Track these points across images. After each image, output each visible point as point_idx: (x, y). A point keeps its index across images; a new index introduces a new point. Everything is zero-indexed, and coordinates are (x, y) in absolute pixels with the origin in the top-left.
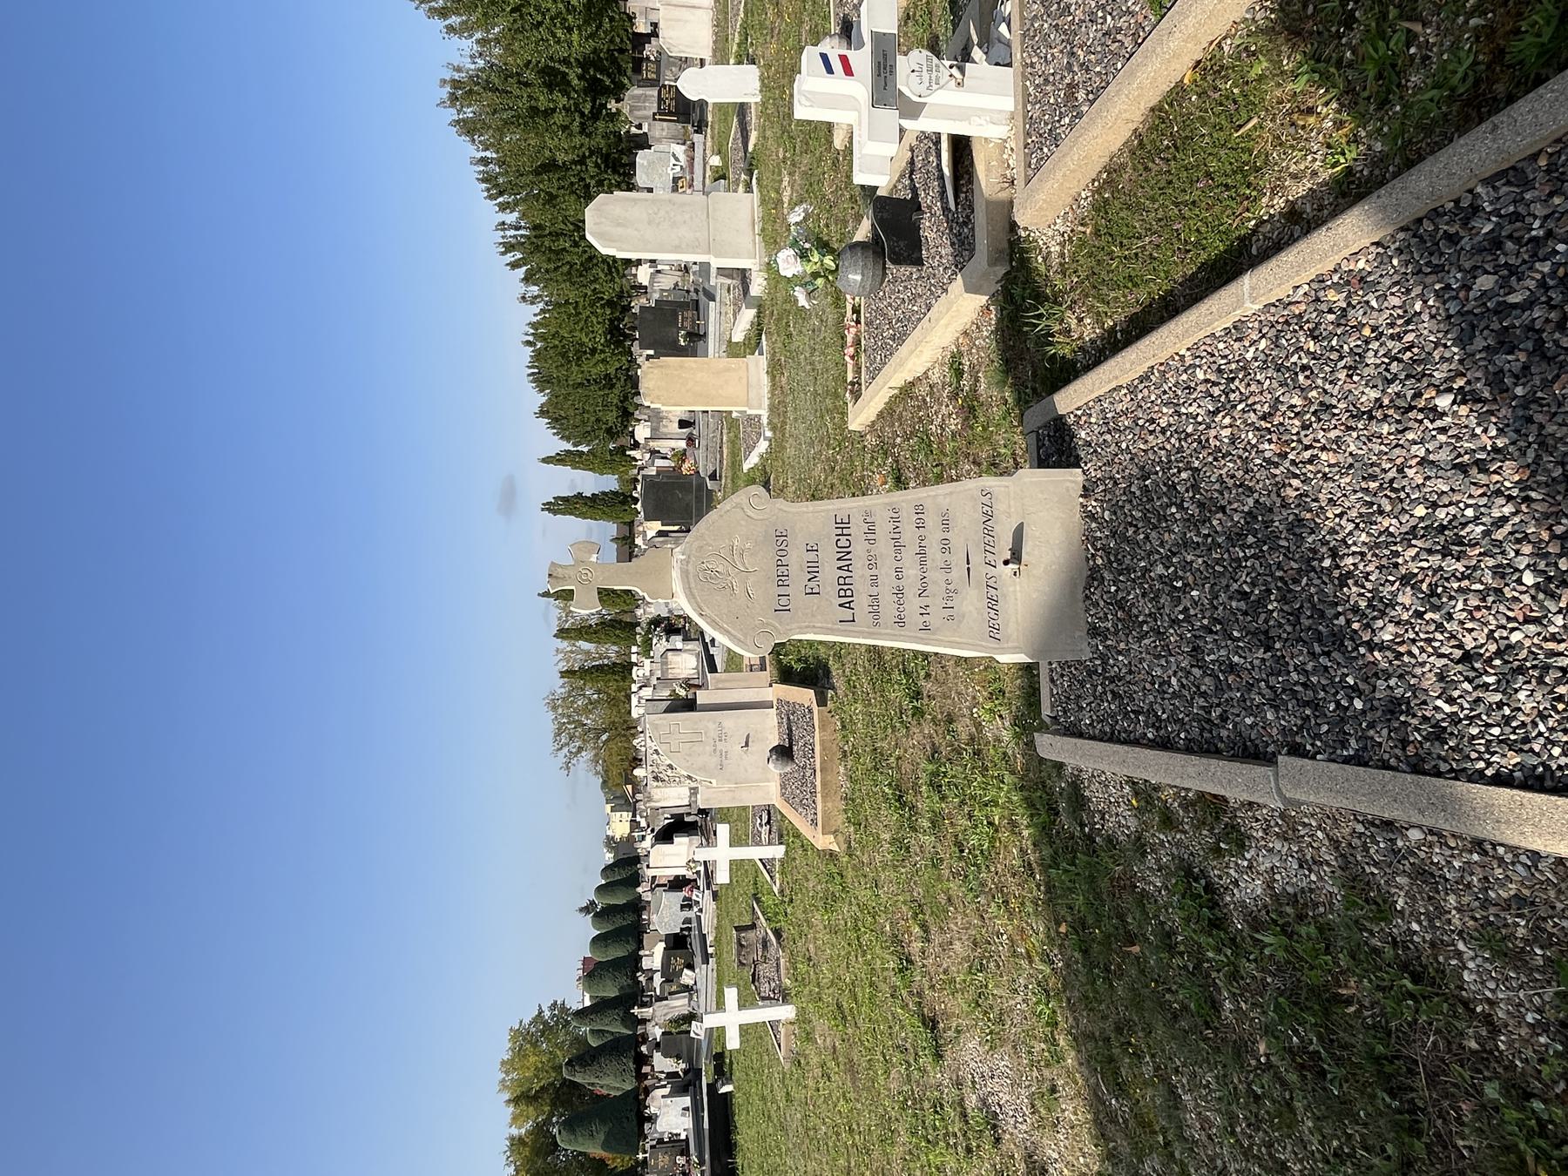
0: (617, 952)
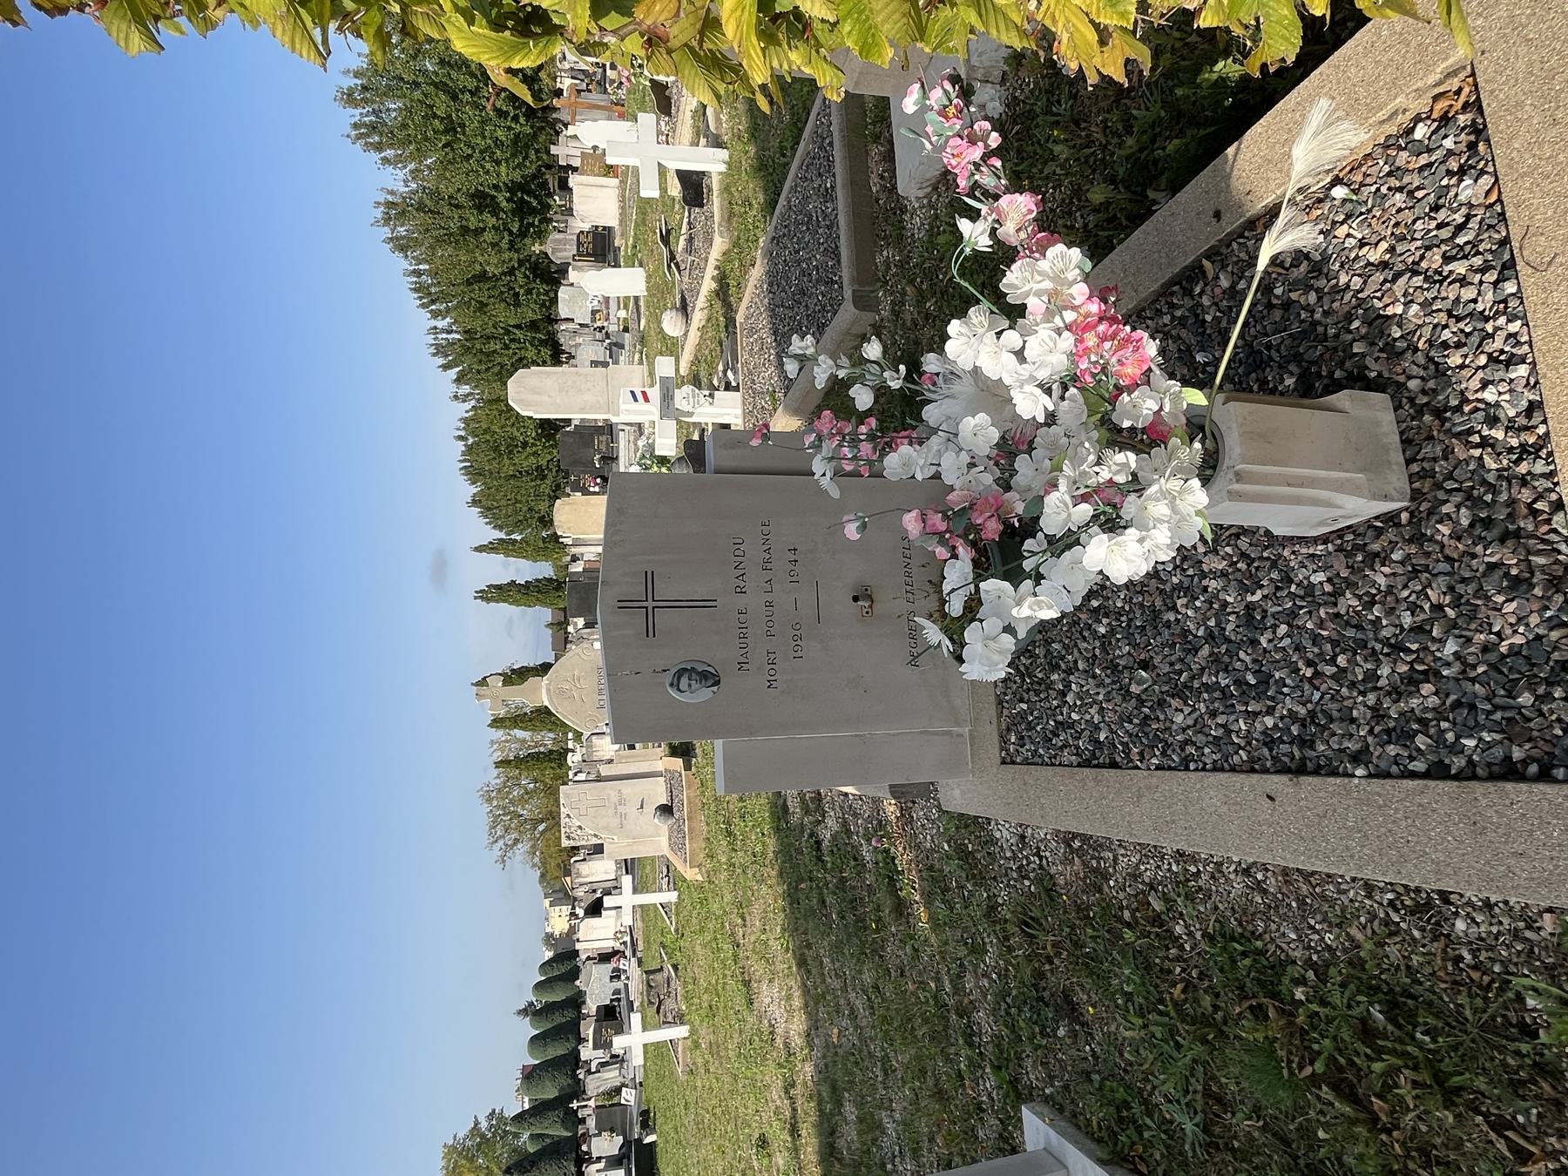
0: (557, 1050)
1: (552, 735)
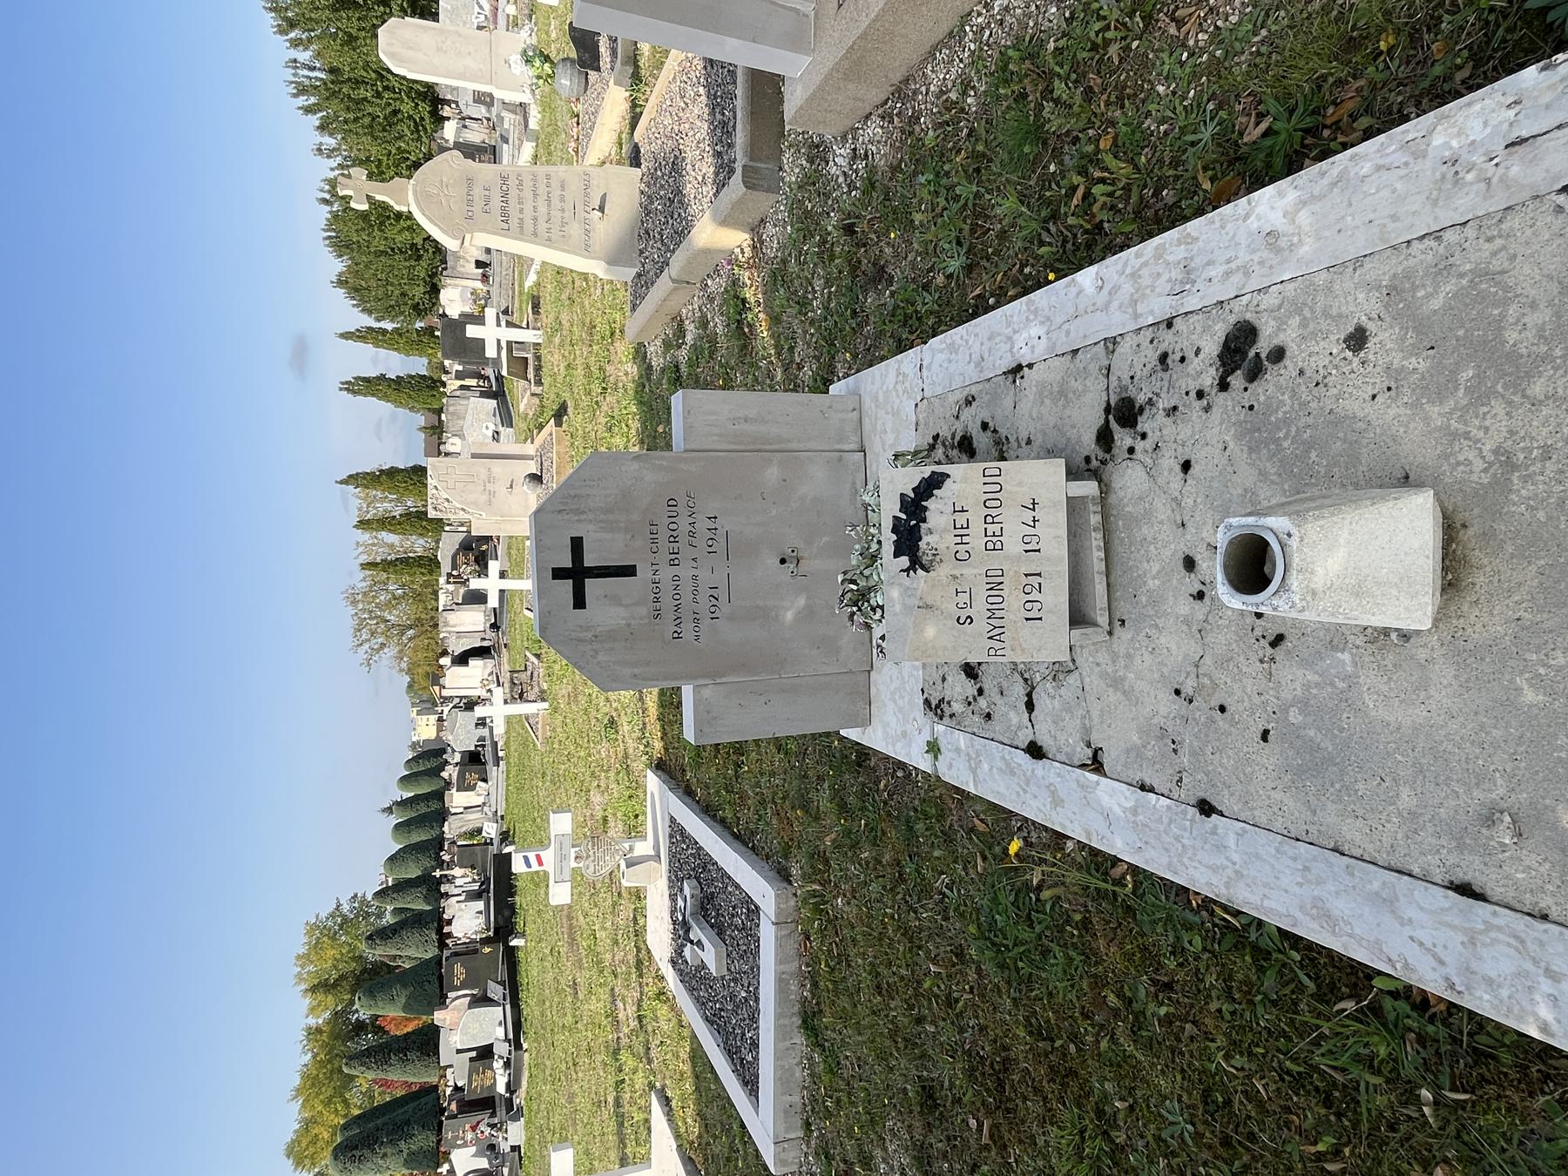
1: (421, 541)
